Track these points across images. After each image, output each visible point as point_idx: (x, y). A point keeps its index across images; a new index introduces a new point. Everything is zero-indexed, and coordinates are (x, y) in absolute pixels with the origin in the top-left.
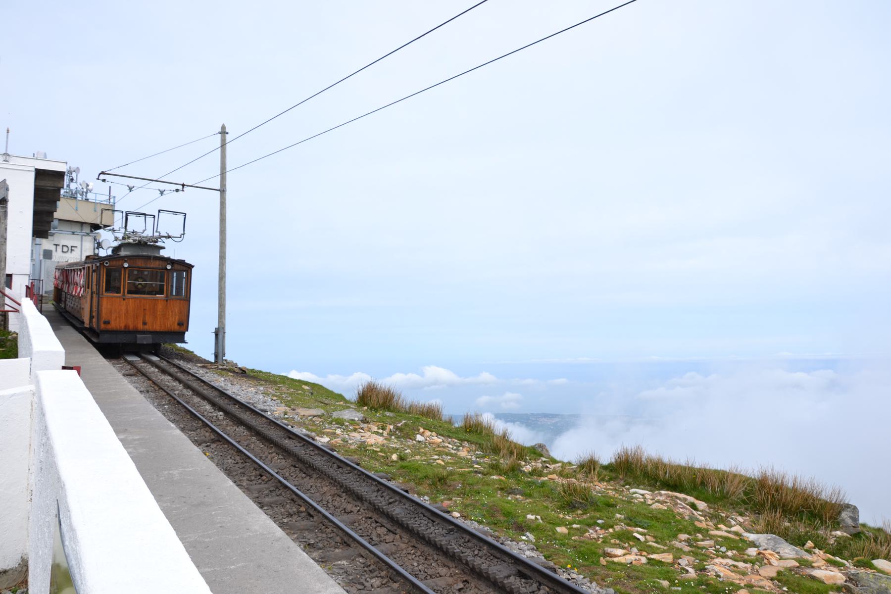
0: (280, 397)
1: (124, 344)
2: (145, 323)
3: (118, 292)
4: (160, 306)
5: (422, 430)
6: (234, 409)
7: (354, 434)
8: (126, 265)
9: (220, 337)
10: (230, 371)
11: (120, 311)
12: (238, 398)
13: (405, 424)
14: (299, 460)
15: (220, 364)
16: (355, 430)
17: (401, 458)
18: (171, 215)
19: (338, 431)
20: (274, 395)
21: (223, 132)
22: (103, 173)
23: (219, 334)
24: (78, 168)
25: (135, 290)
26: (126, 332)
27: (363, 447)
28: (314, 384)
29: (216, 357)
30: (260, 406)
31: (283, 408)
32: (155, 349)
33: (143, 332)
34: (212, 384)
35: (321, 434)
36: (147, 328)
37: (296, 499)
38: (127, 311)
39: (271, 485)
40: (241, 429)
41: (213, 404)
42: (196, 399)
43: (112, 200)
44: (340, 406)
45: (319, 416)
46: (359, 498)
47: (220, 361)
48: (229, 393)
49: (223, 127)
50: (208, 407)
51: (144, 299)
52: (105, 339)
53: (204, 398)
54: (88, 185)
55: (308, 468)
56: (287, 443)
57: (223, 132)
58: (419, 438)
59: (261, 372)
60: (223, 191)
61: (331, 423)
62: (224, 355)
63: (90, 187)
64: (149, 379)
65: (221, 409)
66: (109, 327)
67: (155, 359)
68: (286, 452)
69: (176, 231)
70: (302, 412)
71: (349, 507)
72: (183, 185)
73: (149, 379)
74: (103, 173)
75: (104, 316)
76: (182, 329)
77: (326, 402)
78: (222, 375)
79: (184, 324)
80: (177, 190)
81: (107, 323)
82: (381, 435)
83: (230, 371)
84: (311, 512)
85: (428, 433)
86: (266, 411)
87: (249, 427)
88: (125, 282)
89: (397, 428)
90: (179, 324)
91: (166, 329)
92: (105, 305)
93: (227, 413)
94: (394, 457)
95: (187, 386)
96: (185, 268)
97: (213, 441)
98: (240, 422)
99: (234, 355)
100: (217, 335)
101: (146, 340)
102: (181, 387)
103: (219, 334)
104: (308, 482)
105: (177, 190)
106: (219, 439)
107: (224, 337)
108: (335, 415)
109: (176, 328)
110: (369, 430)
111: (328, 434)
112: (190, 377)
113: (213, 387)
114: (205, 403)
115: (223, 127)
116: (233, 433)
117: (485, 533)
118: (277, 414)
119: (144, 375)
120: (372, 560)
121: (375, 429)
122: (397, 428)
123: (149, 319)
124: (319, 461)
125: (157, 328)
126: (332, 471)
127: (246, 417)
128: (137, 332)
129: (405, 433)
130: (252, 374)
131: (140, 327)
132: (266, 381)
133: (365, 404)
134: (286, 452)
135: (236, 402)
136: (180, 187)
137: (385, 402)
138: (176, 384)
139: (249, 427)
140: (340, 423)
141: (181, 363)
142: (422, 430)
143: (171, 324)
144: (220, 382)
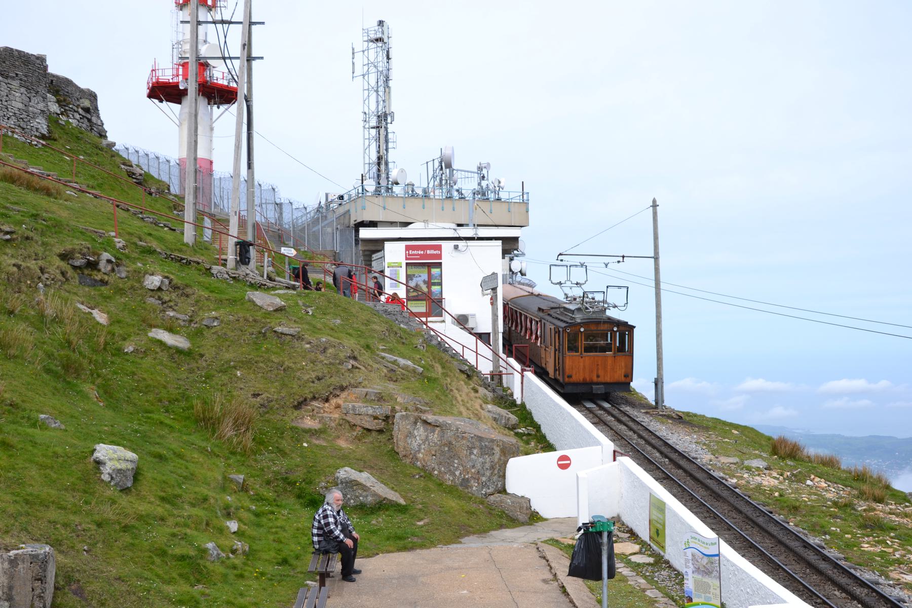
0: (708, 446)
1: (583, 393)
2: (598, 376)
3: (577, 351)
4: (610, 362)
5: (812, 477)
6: (674, 456)
7: (757, 478)
8: (582, 330)
9: (659, 386)
10: (669, 417)
11: (580, 367)
12: (677, 447)
13: (800, 472)
14: (713, 492)
15: (657, 408)
16: (759, 475)
17: (781, 495)
18: (616, 289)
19: (746, 476)
20: (704, 444)
21: (655, 205)
22: (561, 254)
23: (658, 383)
24: (489, 164)
25: (588, 349)
26: (585, 383)
27: (759, 487)
28: (746, 427)
29: (657, 403)
30: (693, 455)
31: (709, 456)
32: (606, 397)
33: (597, 384)
34: (657, 433)
35: (733, 476)
36: (600, 380)
37: (709, 511)
38: (584, 367)
39: (697, 504)
40: (680, 471)
41: (661, 453)
42: (649, 448)
43: (525, 196)
44: (755, 454)
45: (735, 464)
46: (740, 512)
47: (660, 407)
48: (670, 442)
49: (654, 201)
50: (658, 454)
51: (598, 356)
52: (569, 390)
53: (654, 447)
54: (500, 182)
55: (717, 497)
56: (709, 482)
57: (655, 205)
58: (809, 482)
59: (695, 415)
60: (656, 258)
61: (742, 469)
62: (663, 402)
63: (501, 185)
64: (612, 429)
65: (666, 457)
66: (571, 380)
67: (607, 405)
68: (707, 487)
69: (620, 302)
70: (724, 460)
71: (735, 516)
72: (623, 257)
73: (612, 429)
74: (561, 254)
75: (568, 372)
76: (627, 381)
77: (745, 450)
78: (662, 423)
79: (629, 376)
80: (619, 262)
81: (570, 377)
82: (778, 479)
83: (669, 417)
84: (716, 516)
85: (817, 479)
86: (696, 458)
87: (685, 471)
88: (582, 343)
89: (793, 475)
90: (625, 376)
91: (615, 381)
92: (568, 362)
93: (671, 460)
94: (777, 494)
95: (640, 437)
96: (626, 329)
97: (664, 479)
98: (679, 467)
99: (672, 402)
100: (656, 385)
101: (599, 390)
102: (635, 437)
103: (658, 383)
104: (717, 504)
105: (619, 262)
106: (668, 477)
107: (662, 387)
108: (746, 463)
109: (623, 379)
110: (770, 475)
111: (737, 477)
112: (639, 427)
113: (658, 438)
114: (655, 451)
115: (654, 201)
116: (676, 474)
117: (799, 532)
118: (704, 461)
119: (605, 424)
120: (738, 535)
121: (775, 474)
122: (793, 475)
123: (601, 373)
124: (725, 494)
125: (608, 379)
126: (732, 500)
127: (682, 462)
128: (592, 383)
129: (799, 478)
130: (687, 419)
131: (595, 379)
132: (699, 427)
133: (776, 454)
134: (707, 487)
135: (676, 451)
136: (621, 259)
137: (791, 453)
138: (631, 433)
139: (685, 471)
140: (749, 469)
141: (627, 409)
142: (812, 477)
143: (619, 376)
144: (662, 430)
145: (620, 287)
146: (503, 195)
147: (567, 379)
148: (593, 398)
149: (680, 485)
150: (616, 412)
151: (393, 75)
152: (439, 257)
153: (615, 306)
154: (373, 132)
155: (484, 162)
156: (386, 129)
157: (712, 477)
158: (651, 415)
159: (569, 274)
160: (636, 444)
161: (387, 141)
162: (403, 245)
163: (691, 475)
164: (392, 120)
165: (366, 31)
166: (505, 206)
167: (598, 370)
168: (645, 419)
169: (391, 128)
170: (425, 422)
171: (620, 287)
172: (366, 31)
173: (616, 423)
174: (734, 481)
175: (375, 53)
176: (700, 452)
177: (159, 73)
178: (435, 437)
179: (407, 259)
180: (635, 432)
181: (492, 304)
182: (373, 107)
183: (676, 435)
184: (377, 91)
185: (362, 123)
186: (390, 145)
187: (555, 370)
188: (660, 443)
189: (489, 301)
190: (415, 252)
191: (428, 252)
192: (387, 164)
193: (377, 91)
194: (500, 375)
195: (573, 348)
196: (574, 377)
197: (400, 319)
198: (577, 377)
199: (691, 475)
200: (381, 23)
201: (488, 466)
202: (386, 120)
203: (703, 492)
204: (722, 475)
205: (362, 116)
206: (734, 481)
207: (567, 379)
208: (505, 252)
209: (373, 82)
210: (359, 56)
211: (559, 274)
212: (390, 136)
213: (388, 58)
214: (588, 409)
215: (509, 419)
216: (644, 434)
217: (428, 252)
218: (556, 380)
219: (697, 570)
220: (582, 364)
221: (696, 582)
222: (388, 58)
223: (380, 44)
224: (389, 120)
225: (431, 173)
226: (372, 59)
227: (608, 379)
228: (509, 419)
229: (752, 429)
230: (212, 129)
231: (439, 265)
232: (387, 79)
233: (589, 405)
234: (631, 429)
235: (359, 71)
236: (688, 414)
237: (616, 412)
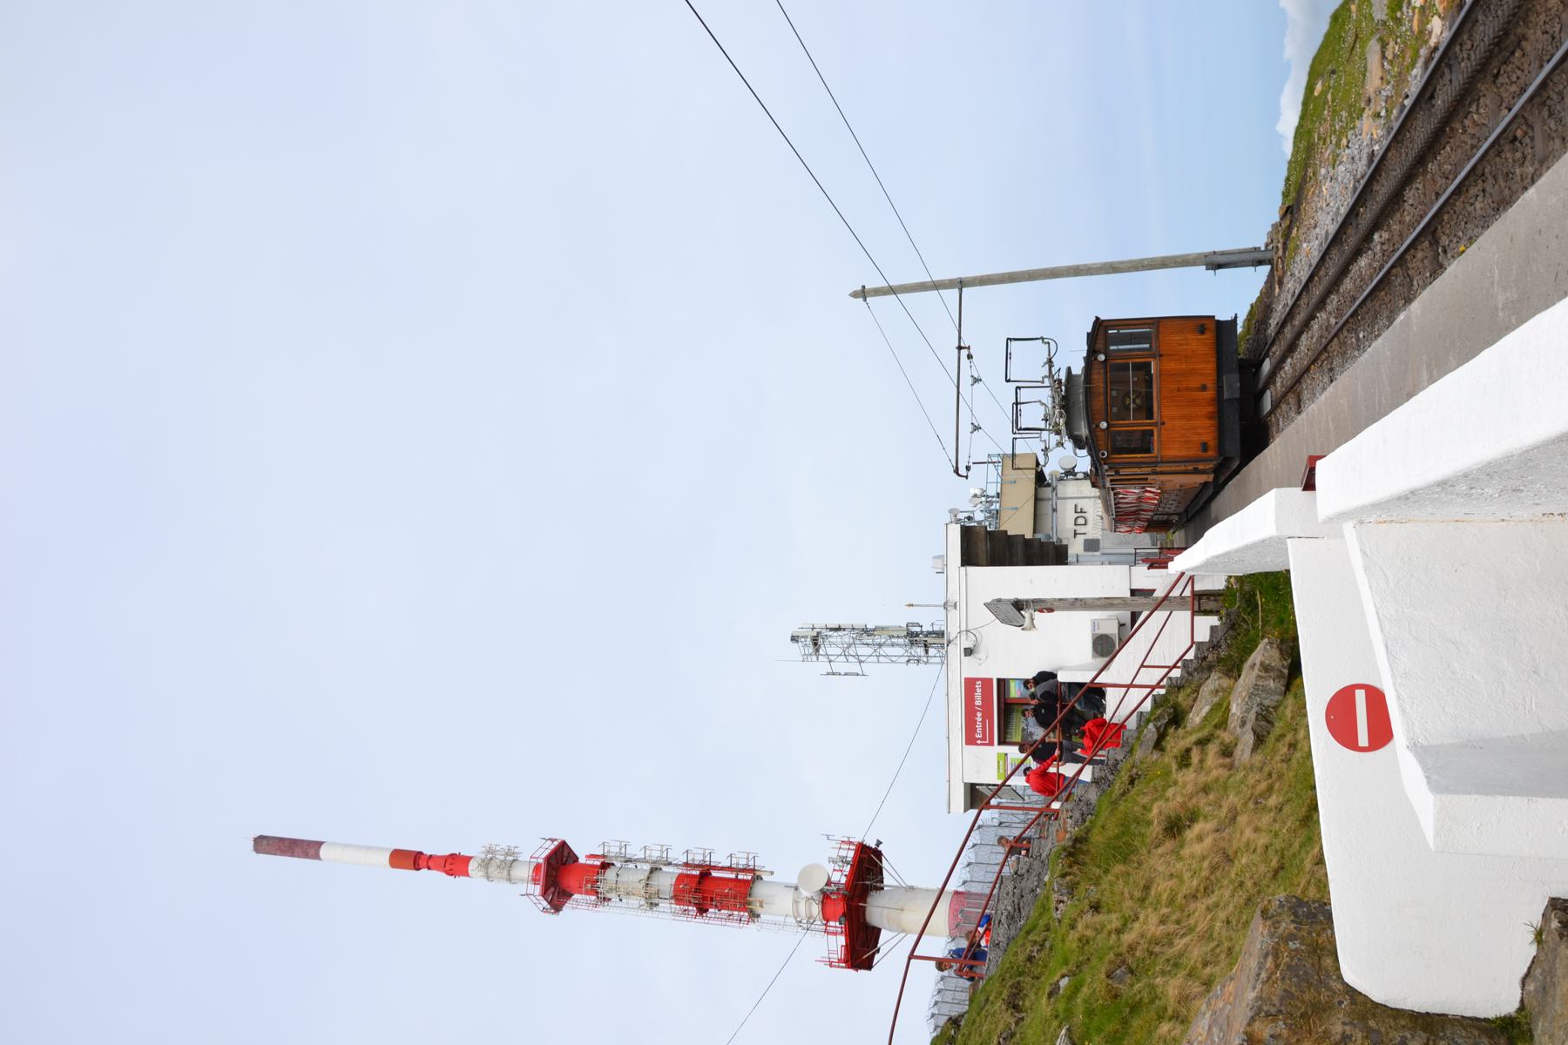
0: (1342, 133)
2: (1204, 388)
3: (1151, 433)
4: (1172, 365)
6: (1367, 215)
8: (1104, 425)
12: (1343, 211)
15: (1273, 257)
18: (1013, 363)
20: (1338, 145)
21: (863, 294)
22: (956, 471)
23: (1216, 262)
26: (1220, 415)
29: (1260, 263)
32: (1249, 368)
33: (1220, 389)
34: (1314, 262)
35: (1423, 34)
36: (1211, 385)
38: (1182, 417)
40: (1410, 195)
41: (1357, 253)
42: (1347, 284)
47: (1269, 255)
48: (1333, 229)
49: (855, 295)
50: (1363, 262)
51: (1160, 391)
52: (1233, 447)
53: (1344, 272)
56: (1441, 102)
59: (1287, 179)
60: (961, 284)
62: (1256, 249)
63: (978, 492)
64: (1307, 370)
65: (1368, 238)
67: (1267, 366)
69: (1040, 352)
70: (1373, 82)
72: (960, 348)
73: (1307, 370)
74: (956, 471)
75: (1194, 452)
76: (1212, 326)
78: (1297, 247)
79: (1202, 324)
80: (970, 357)
83: (1287, 235)
87: (1407, 180)
88: (1134, 424)
90: (1202, 332)
92: (1174, 451)
93: (1376, 225)
95: (1321, 304)
96: (1101, 333)
97: (1435, 242)
98: (1396, 198)
100: (1220, 266)
102: (1322, 316)
103: (1216, 262)
105: (970, 357)
106: (1431, 232)
107: (1223, 253)
109: (1209, 337)
111: (1425, 20)
113: (1323, 259)
114: (1354, 269)
115: (855, 295)
116: (1418, 207)
118: (1378, 133)
119: (1298, 380)
123: (1195, 382)
127: (1383, 190)
128: (1219, 399)
130: (1293, 195)
131: (1210, 394)
135: (1353, 212)
136: (964, 353)
138: (1315, 325)
139: (1407, 180)
141: (1274, 322)
143: (1202, 345)
144: (1310, 248)
145: (1008, 356)
146: (992, 491)
147: (1211, 453)
148: (1252, 392)
149: (1458, 191)
150: (1277, 350)
151: (859, 622)
152: (987, 682)
153: (1050, 362)
154: (932, 651)
156: (929, 634)
157: (1427, 94)
158: (1284, 273)
160: (1339, 315)
162: (1085, 618)
163: (1421, 161)
164: (918, 625)
165: (806, 657)
166: (1008, 488)
167: (1191, 390)
168: (1292, 286)
171: (1008, 356)
172: (806, 657)
173: (1296, 355)
174: (1436, 25)
175: (831, 648)
176: (1354, 150)
177: (835, 957)
179: (991, 744)
180: (1312, 317)
181: (1051, 610)
182: (900, 651)
183: (1321, 216)
184: (880, 645)
185: (922, 665)
187: (1196, 471)
188: (1334, 254)
189: (1046, 615)
190: (979, 727)
191: (978, 703)
193: (880, 645)
194: (1199, 596)
195: (1143, 443)
196: (1204, 438)
197: (1030, 883)
198: (1205, 431)
199: (1421, 161)
200: (794, 639)
202: (917, 635)
203: (1480, 112)
204: (1417, 71)
205: (912, 666)
206: (1436, 25)
207: (1211, 453)
209: (869, 651)
210: (836, 667)
213: (838, 629)
214: (1276, 405)
215: (1266, 668)
216: (1317, 291)
217: (978, 703)
218: (1217, 471)
220: (1178, 423)
222: (838, 629)
223: (820, 641)
226: (839, 651)
227: (1209, 367)
228: (1266, 668)
229: (1315, 59)
230: (912, 888)
231: (1003, 684)
232: (866, 631)
233: (1267, 404)
234: (1306, 325)
235: (855, 668)
236: (1285, 195)
237: (1277, 350)
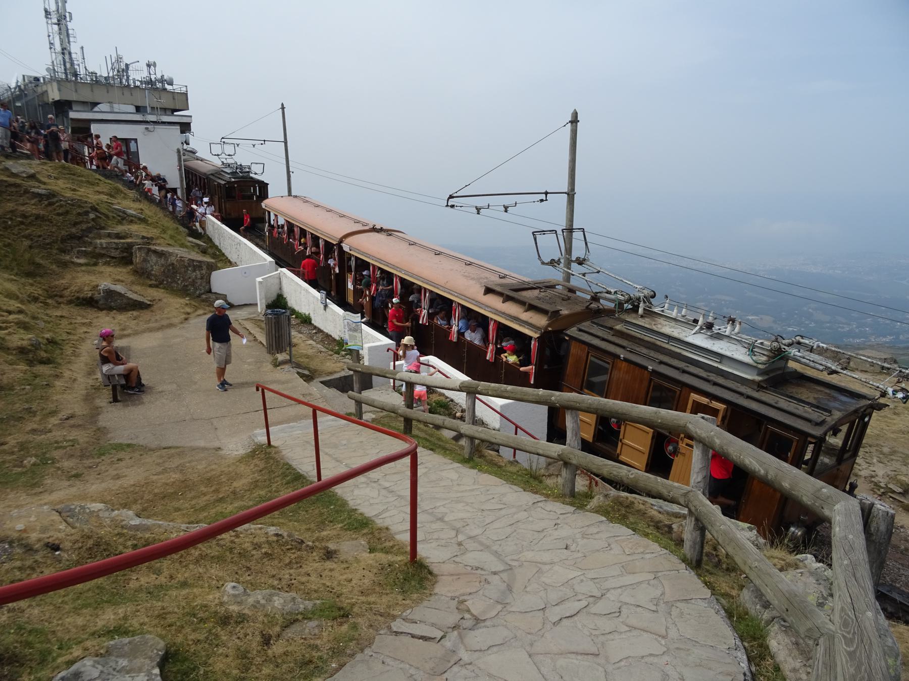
49: (282, 105)
57: (283, 108)
60: (286, 142)
69: (259, 171)
80: (542, 201)
105: (542, 201)
115: (282, 105)
155: (152, 61)
159: (223, 149)
161: (68, 35)
169: (70, 25)
170: (155, 252)
178: (162, 261)
186: (71, 39)
192: (70, 53)
201: (199, 276)
208: (182, 132)
211: (217, 149)
212: (70, 32)
219: (350, 330)
221: (350, 335)
224: (68, 19)
225: (110, 66)
